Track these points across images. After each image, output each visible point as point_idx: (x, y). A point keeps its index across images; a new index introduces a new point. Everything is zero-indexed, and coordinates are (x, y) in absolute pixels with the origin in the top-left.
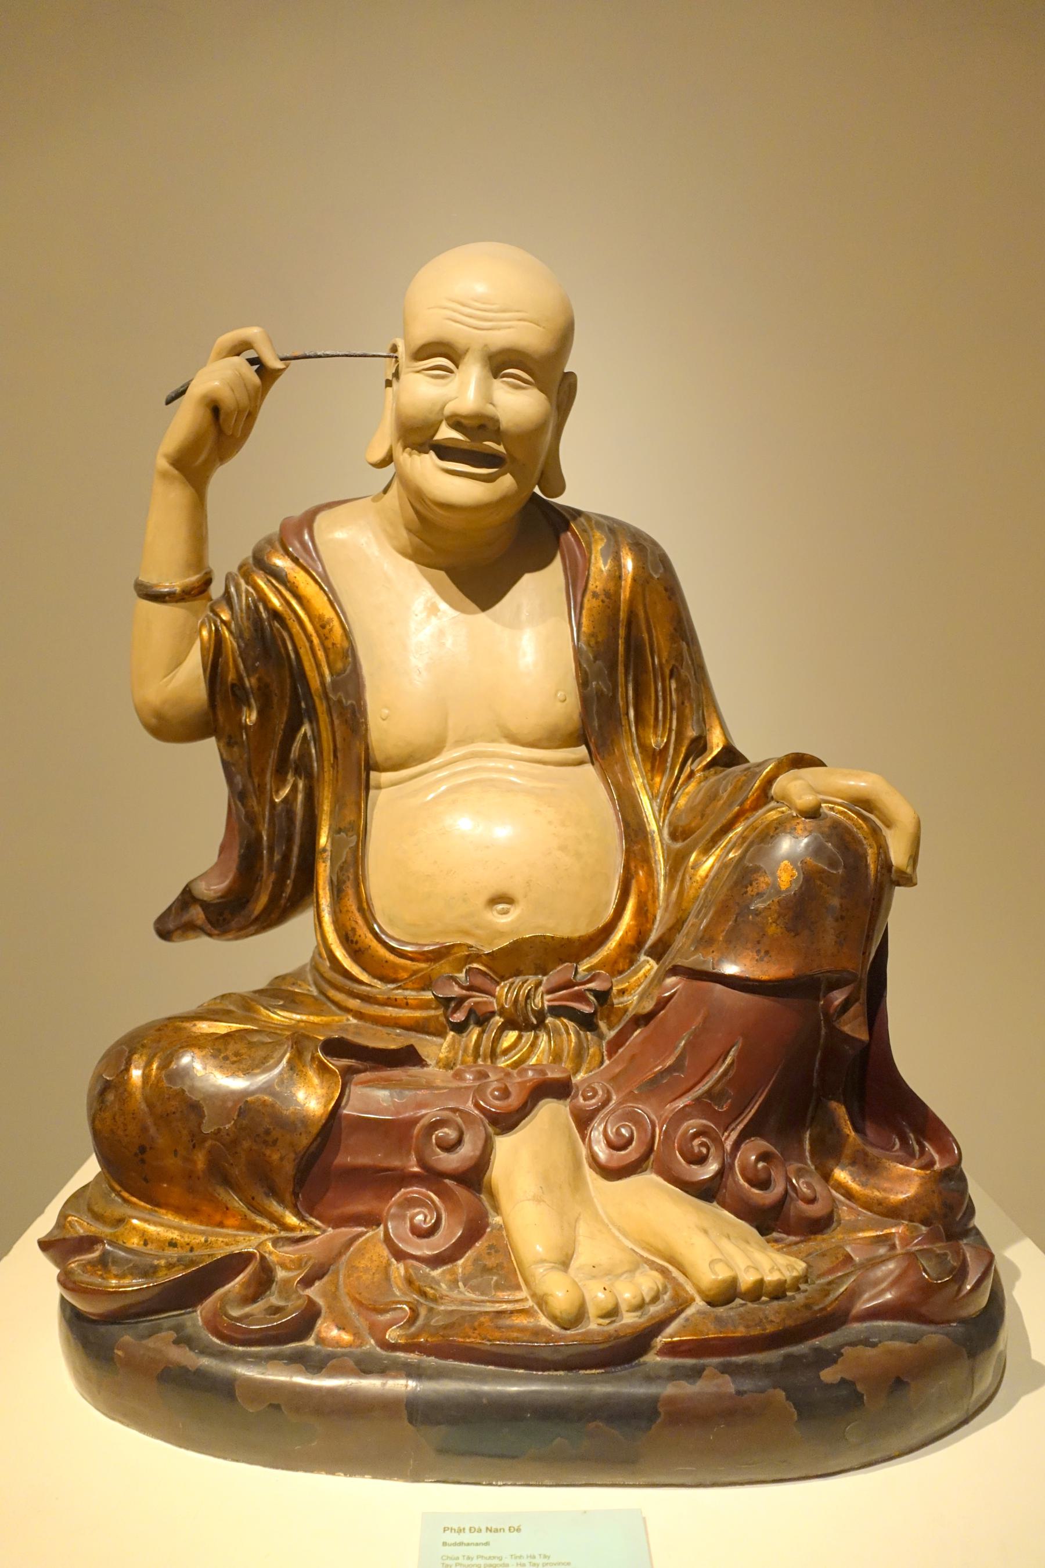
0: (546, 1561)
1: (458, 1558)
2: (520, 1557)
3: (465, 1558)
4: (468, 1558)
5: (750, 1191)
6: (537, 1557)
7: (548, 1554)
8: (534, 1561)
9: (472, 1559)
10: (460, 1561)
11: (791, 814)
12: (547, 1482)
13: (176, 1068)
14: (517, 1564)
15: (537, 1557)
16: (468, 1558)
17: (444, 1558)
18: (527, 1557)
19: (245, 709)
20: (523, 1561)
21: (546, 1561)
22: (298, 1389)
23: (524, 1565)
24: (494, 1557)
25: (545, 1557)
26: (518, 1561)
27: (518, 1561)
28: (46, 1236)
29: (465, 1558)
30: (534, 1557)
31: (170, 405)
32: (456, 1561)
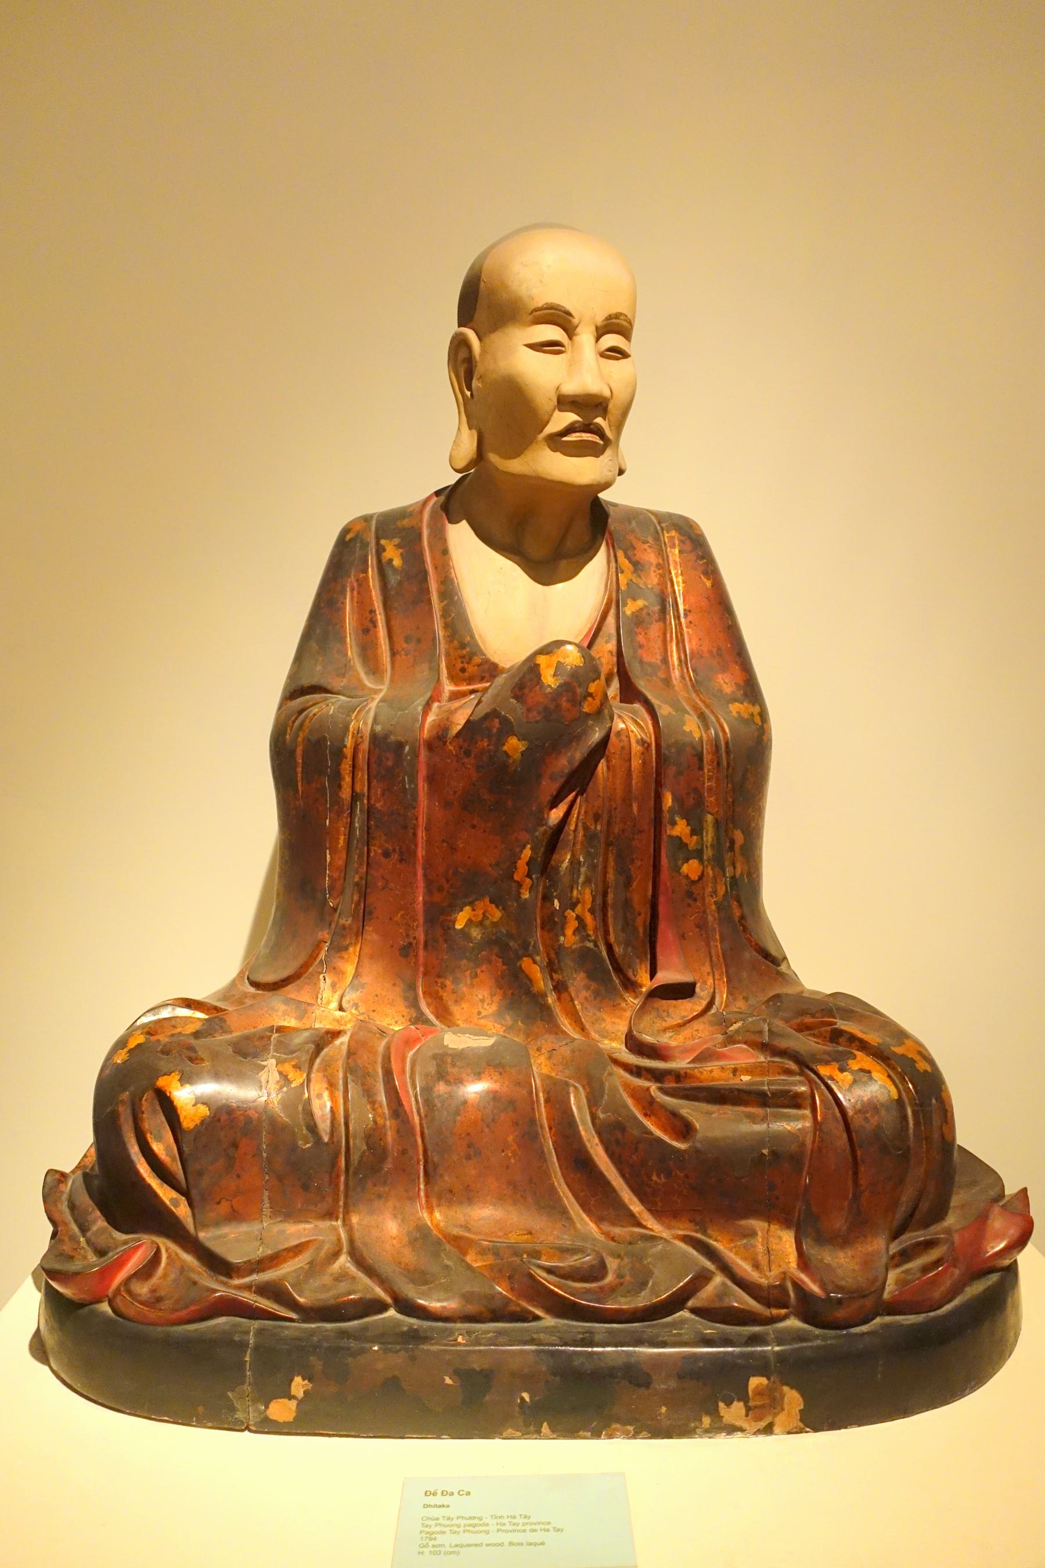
0: (526, 1521)
1: (438, 1519)
2: (501, 1517)
3: (522, 1516)
4: (449, 1519)
5: (339, 1208)
6: (518, 1517)
7: (528, 1514)
8: (514, 1521)
9: (452, 1519)
10: (441, 1521)
11: (632, 952)
12: (210, 1424)
13: (382, 729)
14: (541, 1530)
15: (518, 1517)
16: (449, 1519)
17: (424, 1519)
18: (508, 1517)
19: (599, 536)
20: (503, 1521)
21: (526, 1521)
22: (943, 1086)
23: (548, 1530)
24: (475, 1518)
25: (525, 1517)
26: (499, 1521)
27: (499, 1521)
28: (605, 501)
29: (522, 1516)
30: (515, 1517)
31: (603, 361)
32: (436, 1522)
